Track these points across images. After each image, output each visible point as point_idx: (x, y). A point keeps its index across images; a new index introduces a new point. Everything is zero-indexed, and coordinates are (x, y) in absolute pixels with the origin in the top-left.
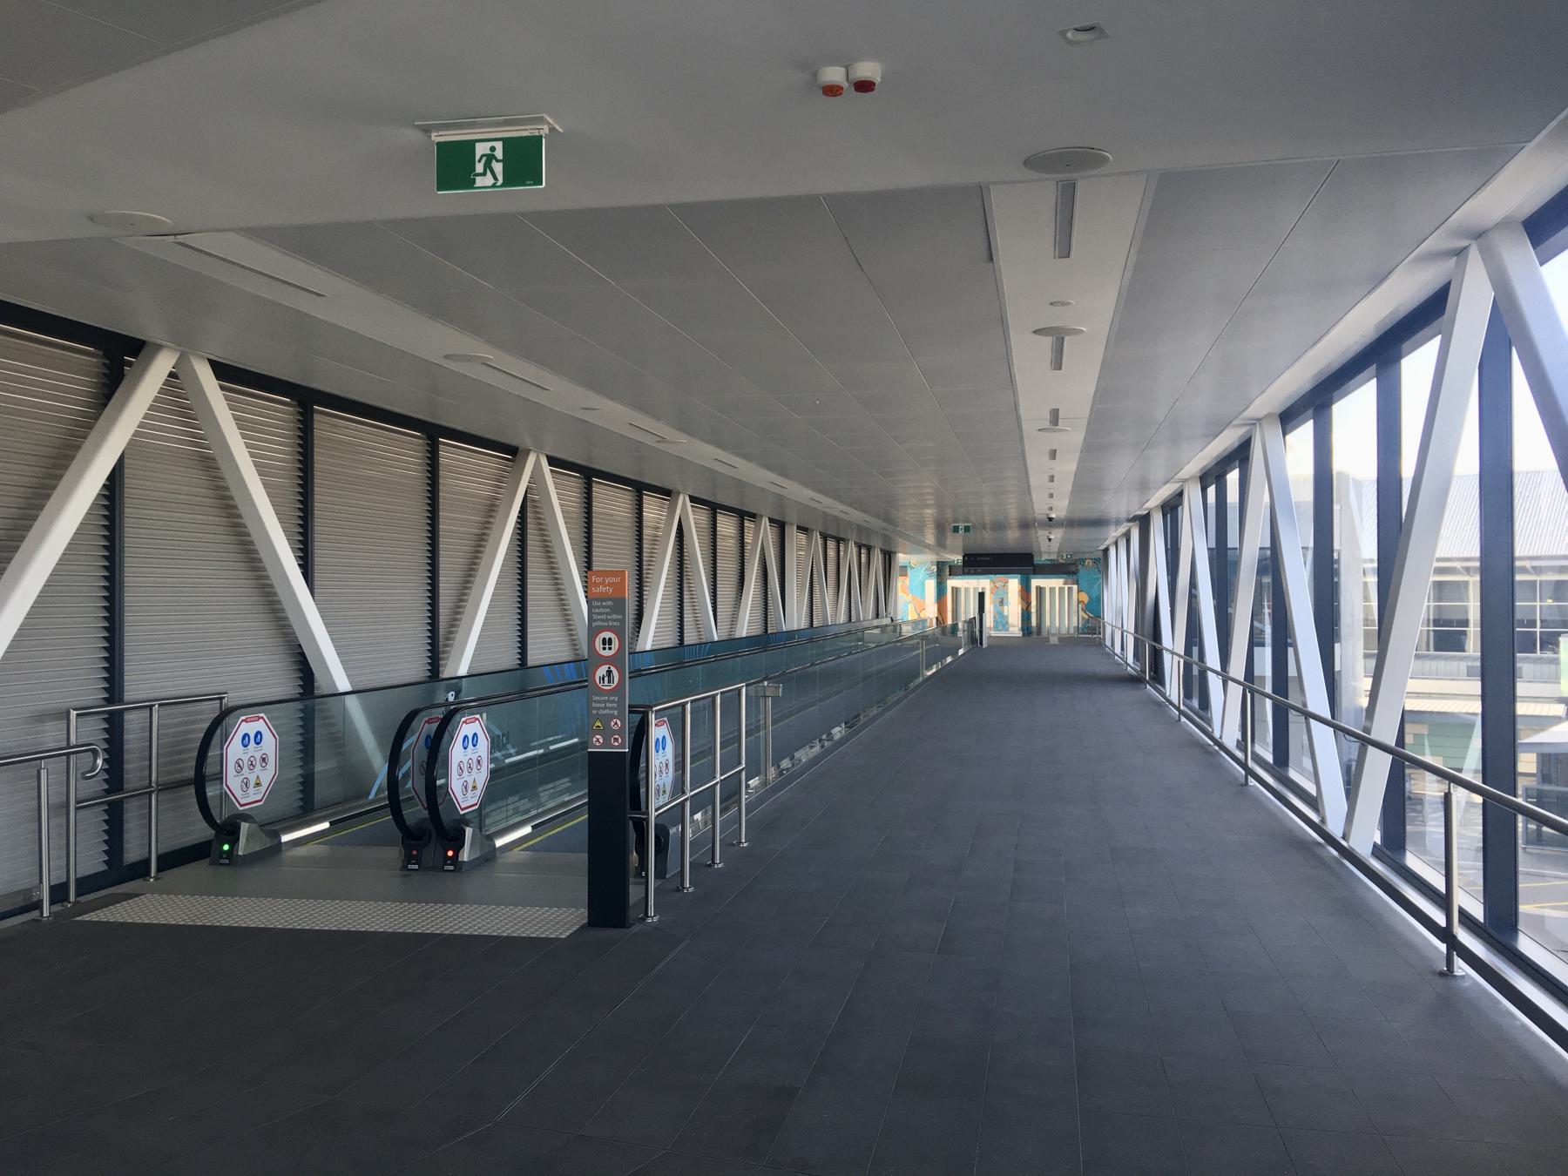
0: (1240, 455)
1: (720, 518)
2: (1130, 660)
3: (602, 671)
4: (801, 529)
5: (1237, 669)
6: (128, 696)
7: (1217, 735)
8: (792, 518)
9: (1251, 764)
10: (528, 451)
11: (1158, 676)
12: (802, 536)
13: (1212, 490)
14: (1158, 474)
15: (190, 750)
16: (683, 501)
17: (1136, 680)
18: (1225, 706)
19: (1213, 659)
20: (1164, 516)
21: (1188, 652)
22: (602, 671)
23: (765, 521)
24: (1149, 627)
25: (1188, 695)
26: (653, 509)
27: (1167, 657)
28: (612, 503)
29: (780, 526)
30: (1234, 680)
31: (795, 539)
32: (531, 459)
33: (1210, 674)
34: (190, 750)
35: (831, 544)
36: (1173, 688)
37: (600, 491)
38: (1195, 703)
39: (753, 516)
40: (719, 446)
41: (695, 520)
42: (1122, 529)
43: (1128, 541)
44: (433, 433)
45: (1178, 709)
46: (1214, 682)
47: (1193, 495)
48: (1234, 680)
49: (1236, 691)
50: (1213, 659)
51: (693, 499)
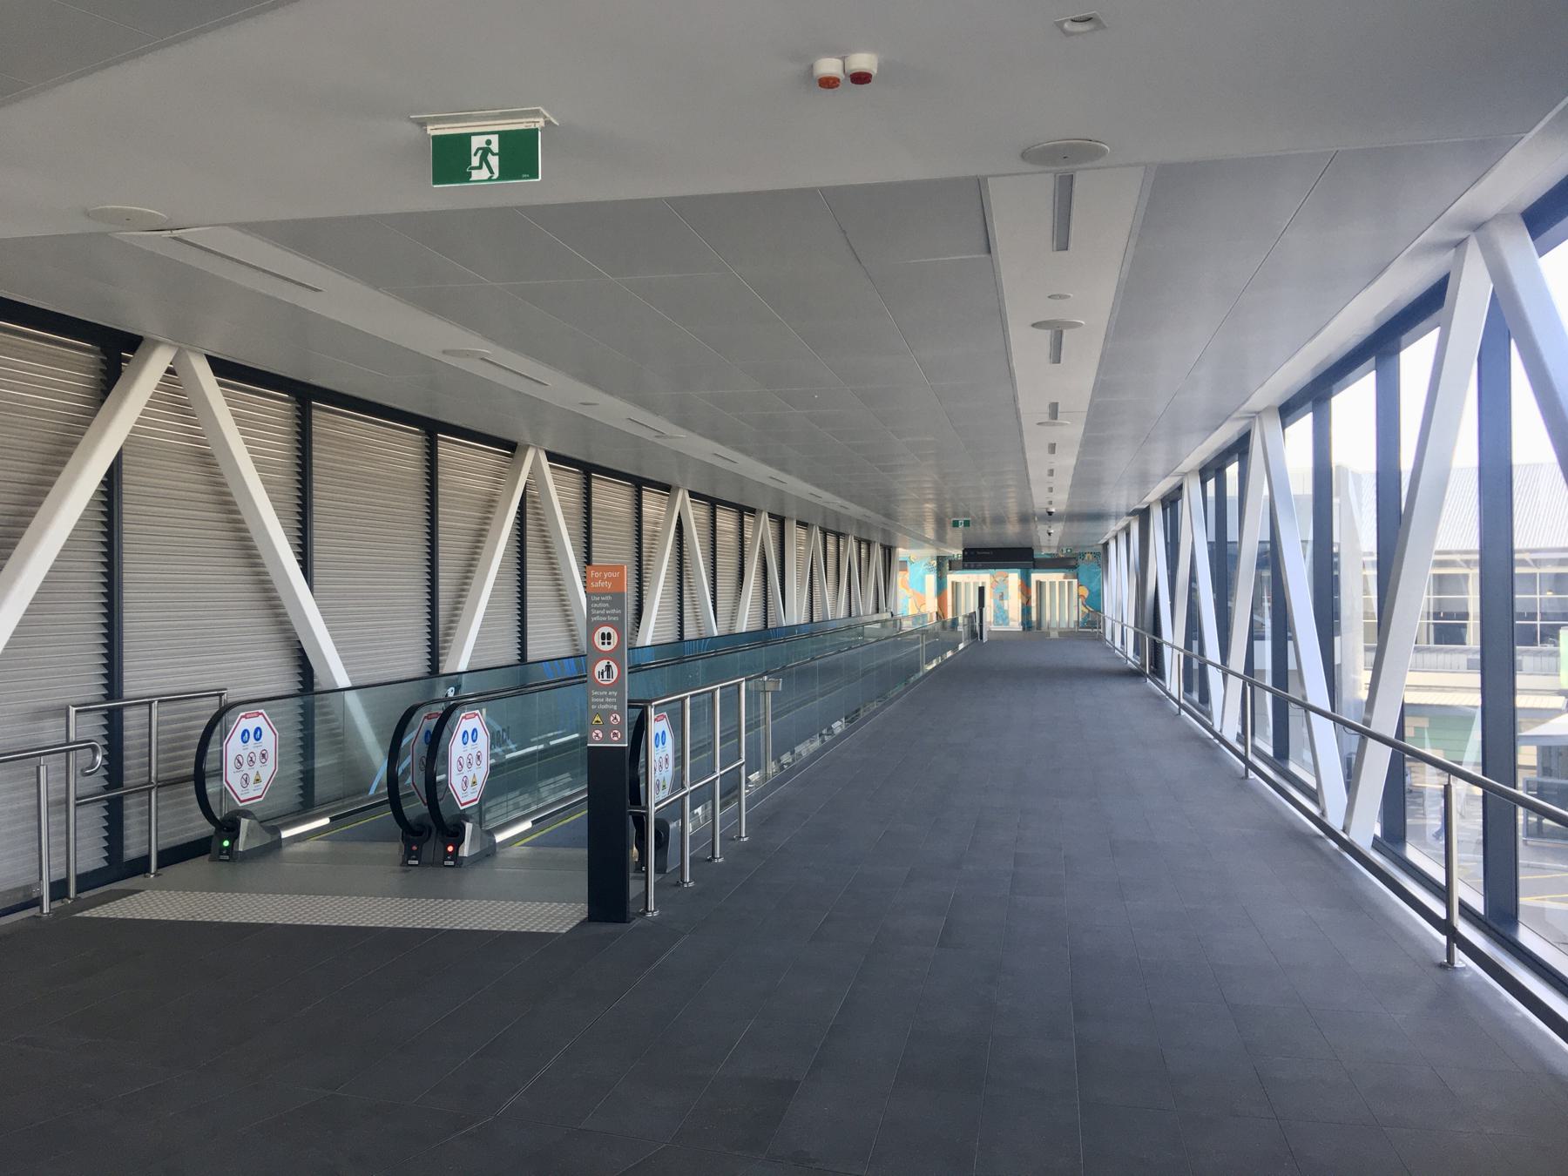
0: (1240, 448)
1: (719, 513)
2: (1131, 654)
5: (1237, 662)
7: (1217, 728)
8: (792, 513)
9: (1251, 757)
10: (527, 447)
11: (1158, 670)
12: (802, 532)
13: (1211, 484)
14: (1158, 468)
16: (682, 496)
17: (1136, 674)
18: (1225, 699)
19: (1213, 652)
23: (765, 517)
24: (1149, 623)
25: (1188, 688)
26: (652, 504)
27: (1167, 651)
28: (611, 499)
29: (780, 521)
31: (794, 533)
32: (530, 455)
36: (1173, 682)
38: (1195, 697)
39: (753, 511)
41: (695, 515)
42: (1122, 523)
43: (1128, 535)
44: (432, 429)
45: (1178, 702)
46: (1214, 676)
47: (1193, 488)
49: (1236, 684)
50: (1213, 652)
51: (692, 494)
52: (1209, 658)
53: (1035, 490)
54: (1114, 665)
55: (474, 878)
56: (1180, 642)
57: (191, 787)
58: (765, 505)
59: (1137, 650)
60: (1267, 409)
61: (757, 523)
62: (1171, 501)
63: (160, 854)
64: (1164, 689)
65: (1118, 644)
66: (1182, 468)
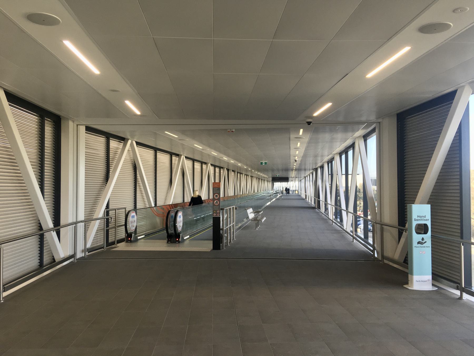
0: (352, 146)
1: (195, 163)
2: (313, 203)
3: (215, 201)
4: (233, 171)
5: (351, 209)
6: (61, 225)
7: (345, 228)
8: (231, 168)
9: (354, 236)
10: (128, 139)
11: (319, 207)
12: (233, 173)
13: (343, 157)
14: (326, 152)
15: (46, 249)
16: (183, 157)
17: (314, 208)
18: (347, 220)
19: (343, 206)
20: (328, 164)
21: (336, 204)
22: (215, 201)
23: (209, 165)
24: (317, 195)
25: (336, 218)
26: (204, 166)
27: (321, 202)
28: (163, 159)
29: (228, 170)
30: (344, 210)
31: (232, 174)
32: (129, 142)
33: (343, 211)
34: (46, 249)
35: (239, 175)
36: (323, 209)
37: (159, 155)
38: (339, 220)
39: (222, 168)
40: (22, 31)
41: (212, 169)
42: (311, 171)
43: (312, 174)
44: (156, 150)
45: (332, 221)
46: (344, 213)
47: (337, 158)
48: (344, 210)
49: (351, 216)
50: (343, 206)
51: (186, 157)
52: (342, 208)
53: (303, 150)
54: (308, 206)
55: (181, 244)
56: (333, 203)
57: (124, 227)
58: (226, 167)
59: (315, 203)
60: (359, 137)
61: (224, 171)
62: (322, 167)
63: (117, 241)
64: (328, 217)
65: (310, 201)
66: (333, 153)
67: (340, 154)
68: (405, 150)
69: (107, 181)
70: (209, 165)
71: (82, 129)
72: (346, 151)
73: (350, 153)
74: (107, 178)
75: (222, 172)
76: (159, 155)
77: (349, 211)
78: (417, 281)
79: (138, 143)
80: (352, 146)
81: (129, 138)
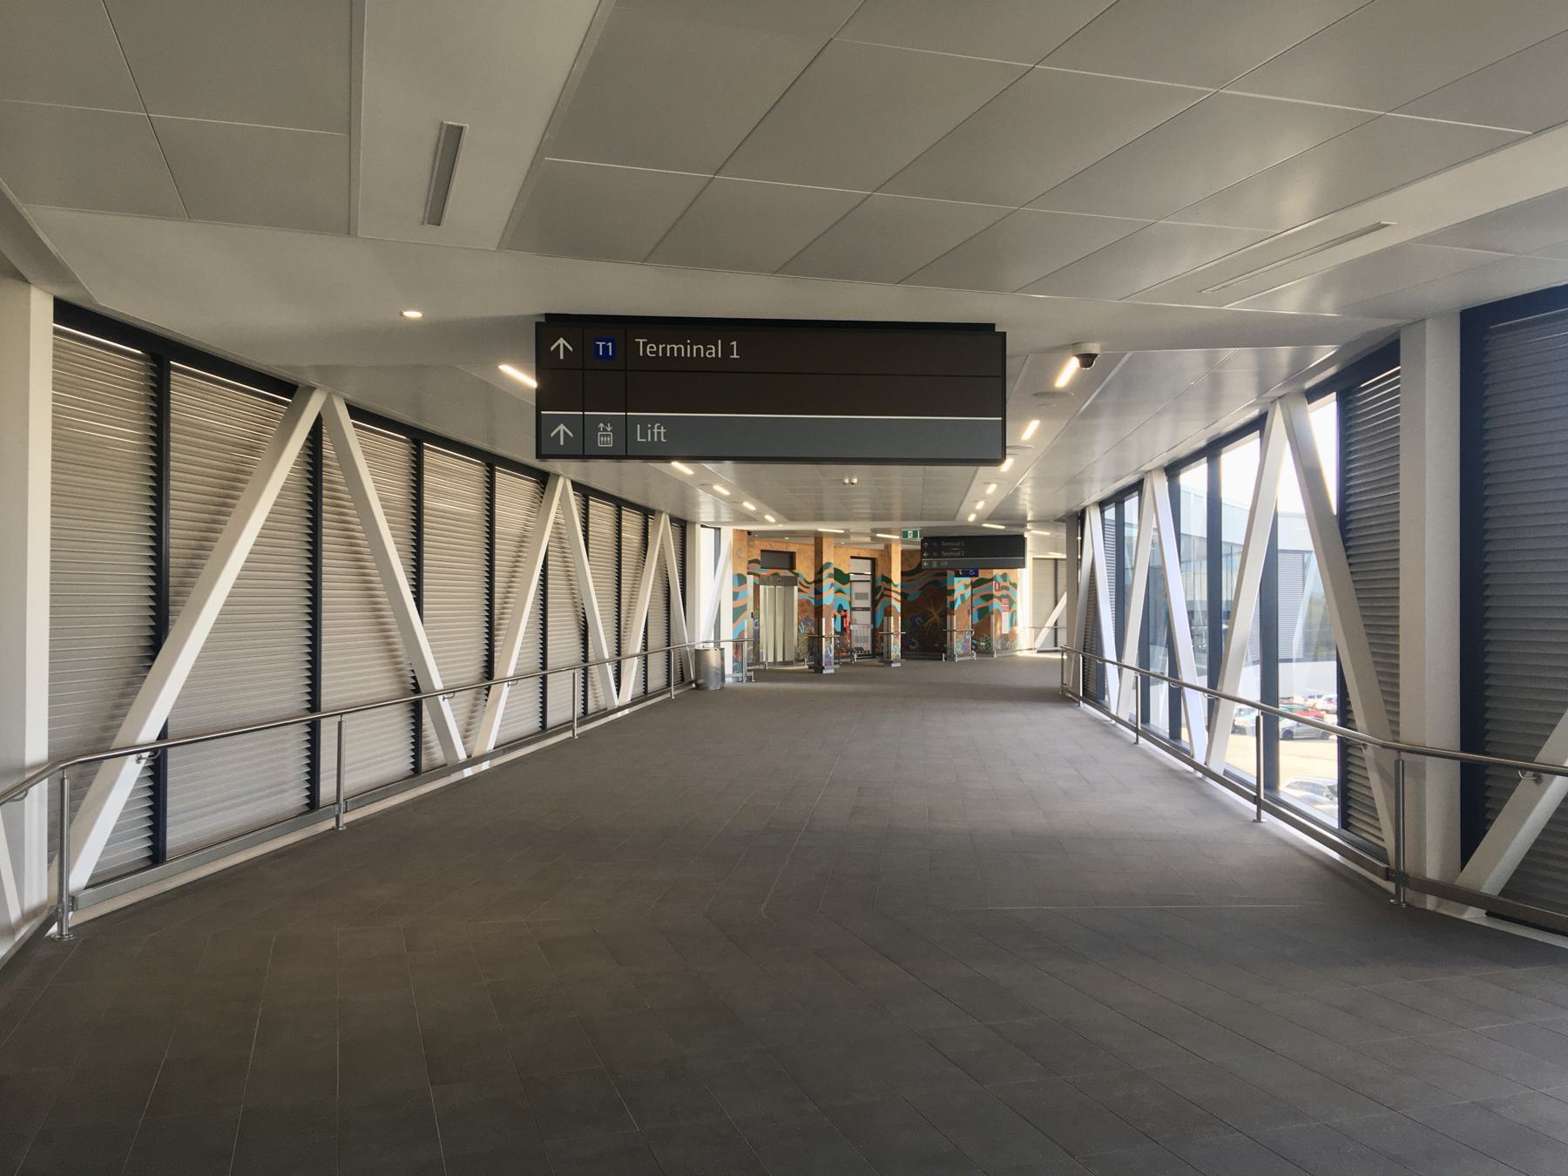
0: (1137, 487)
5: (1131, 655)
44: (418, 438)
46: (1111, 671)
49: (1129, 676)
50: (1110, 652)
67: (1102, 505)
68: (1487, 564)
69: (153, 658)
70: (664, 520)
71: (41, 307)
72: (1118, 499)
73: (1131, 504)
74: (157, 635)
75: (631, 535)
76: (503, 478)
77: (1126, 661)
78: (340, 723)
79: (356, 412)
80: (1137, 487)
81: (314, 383)
